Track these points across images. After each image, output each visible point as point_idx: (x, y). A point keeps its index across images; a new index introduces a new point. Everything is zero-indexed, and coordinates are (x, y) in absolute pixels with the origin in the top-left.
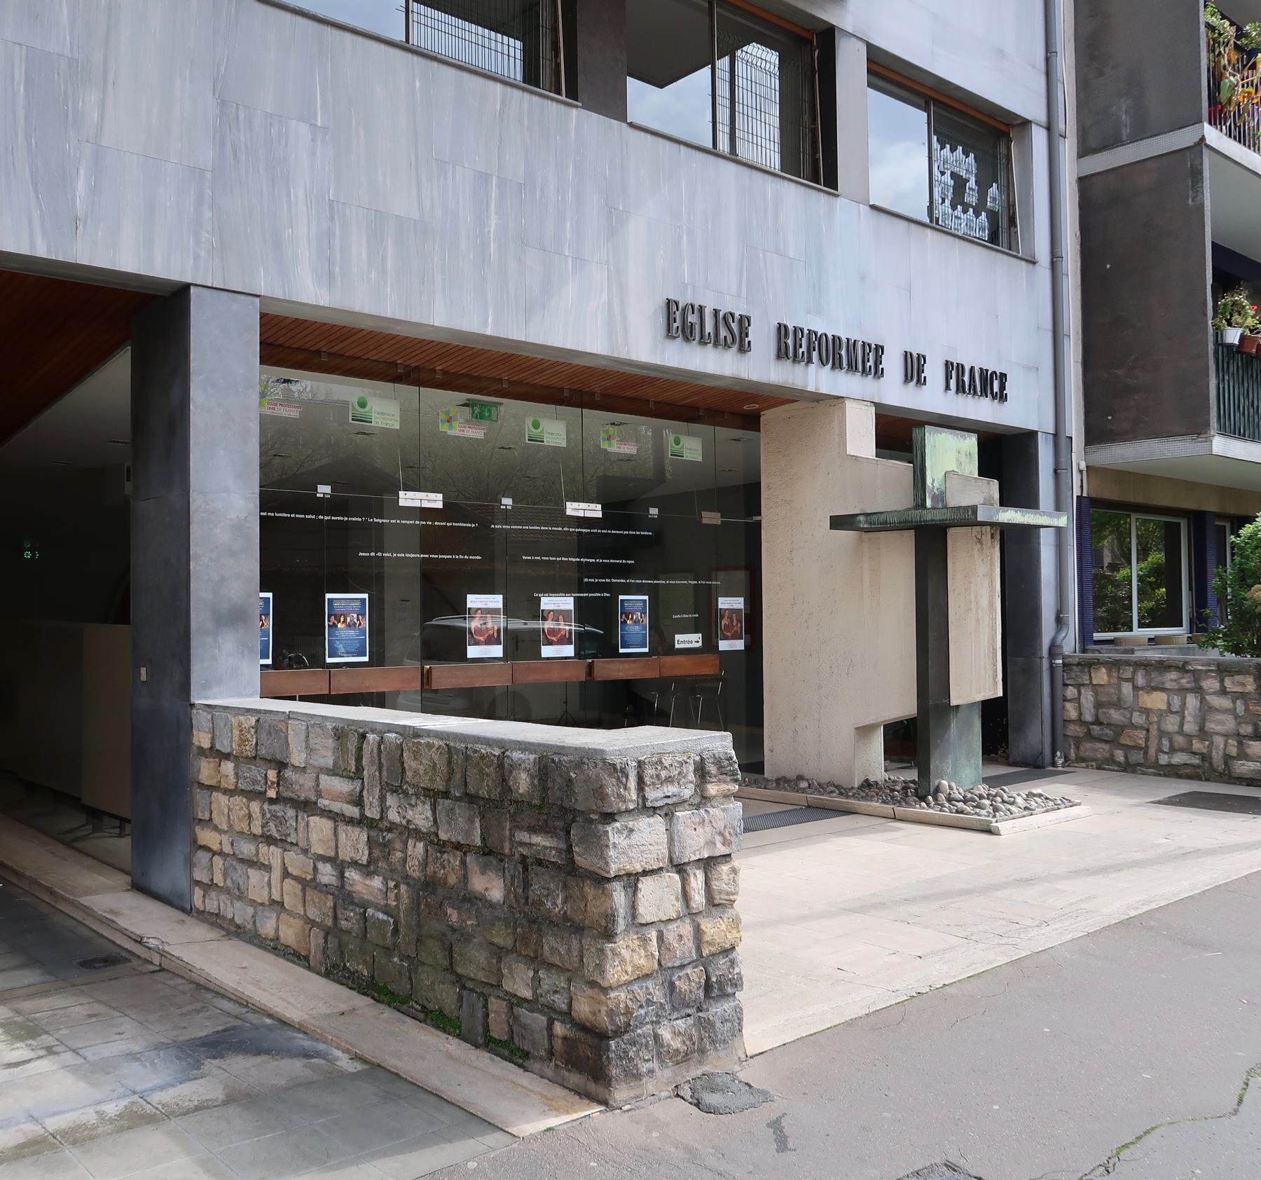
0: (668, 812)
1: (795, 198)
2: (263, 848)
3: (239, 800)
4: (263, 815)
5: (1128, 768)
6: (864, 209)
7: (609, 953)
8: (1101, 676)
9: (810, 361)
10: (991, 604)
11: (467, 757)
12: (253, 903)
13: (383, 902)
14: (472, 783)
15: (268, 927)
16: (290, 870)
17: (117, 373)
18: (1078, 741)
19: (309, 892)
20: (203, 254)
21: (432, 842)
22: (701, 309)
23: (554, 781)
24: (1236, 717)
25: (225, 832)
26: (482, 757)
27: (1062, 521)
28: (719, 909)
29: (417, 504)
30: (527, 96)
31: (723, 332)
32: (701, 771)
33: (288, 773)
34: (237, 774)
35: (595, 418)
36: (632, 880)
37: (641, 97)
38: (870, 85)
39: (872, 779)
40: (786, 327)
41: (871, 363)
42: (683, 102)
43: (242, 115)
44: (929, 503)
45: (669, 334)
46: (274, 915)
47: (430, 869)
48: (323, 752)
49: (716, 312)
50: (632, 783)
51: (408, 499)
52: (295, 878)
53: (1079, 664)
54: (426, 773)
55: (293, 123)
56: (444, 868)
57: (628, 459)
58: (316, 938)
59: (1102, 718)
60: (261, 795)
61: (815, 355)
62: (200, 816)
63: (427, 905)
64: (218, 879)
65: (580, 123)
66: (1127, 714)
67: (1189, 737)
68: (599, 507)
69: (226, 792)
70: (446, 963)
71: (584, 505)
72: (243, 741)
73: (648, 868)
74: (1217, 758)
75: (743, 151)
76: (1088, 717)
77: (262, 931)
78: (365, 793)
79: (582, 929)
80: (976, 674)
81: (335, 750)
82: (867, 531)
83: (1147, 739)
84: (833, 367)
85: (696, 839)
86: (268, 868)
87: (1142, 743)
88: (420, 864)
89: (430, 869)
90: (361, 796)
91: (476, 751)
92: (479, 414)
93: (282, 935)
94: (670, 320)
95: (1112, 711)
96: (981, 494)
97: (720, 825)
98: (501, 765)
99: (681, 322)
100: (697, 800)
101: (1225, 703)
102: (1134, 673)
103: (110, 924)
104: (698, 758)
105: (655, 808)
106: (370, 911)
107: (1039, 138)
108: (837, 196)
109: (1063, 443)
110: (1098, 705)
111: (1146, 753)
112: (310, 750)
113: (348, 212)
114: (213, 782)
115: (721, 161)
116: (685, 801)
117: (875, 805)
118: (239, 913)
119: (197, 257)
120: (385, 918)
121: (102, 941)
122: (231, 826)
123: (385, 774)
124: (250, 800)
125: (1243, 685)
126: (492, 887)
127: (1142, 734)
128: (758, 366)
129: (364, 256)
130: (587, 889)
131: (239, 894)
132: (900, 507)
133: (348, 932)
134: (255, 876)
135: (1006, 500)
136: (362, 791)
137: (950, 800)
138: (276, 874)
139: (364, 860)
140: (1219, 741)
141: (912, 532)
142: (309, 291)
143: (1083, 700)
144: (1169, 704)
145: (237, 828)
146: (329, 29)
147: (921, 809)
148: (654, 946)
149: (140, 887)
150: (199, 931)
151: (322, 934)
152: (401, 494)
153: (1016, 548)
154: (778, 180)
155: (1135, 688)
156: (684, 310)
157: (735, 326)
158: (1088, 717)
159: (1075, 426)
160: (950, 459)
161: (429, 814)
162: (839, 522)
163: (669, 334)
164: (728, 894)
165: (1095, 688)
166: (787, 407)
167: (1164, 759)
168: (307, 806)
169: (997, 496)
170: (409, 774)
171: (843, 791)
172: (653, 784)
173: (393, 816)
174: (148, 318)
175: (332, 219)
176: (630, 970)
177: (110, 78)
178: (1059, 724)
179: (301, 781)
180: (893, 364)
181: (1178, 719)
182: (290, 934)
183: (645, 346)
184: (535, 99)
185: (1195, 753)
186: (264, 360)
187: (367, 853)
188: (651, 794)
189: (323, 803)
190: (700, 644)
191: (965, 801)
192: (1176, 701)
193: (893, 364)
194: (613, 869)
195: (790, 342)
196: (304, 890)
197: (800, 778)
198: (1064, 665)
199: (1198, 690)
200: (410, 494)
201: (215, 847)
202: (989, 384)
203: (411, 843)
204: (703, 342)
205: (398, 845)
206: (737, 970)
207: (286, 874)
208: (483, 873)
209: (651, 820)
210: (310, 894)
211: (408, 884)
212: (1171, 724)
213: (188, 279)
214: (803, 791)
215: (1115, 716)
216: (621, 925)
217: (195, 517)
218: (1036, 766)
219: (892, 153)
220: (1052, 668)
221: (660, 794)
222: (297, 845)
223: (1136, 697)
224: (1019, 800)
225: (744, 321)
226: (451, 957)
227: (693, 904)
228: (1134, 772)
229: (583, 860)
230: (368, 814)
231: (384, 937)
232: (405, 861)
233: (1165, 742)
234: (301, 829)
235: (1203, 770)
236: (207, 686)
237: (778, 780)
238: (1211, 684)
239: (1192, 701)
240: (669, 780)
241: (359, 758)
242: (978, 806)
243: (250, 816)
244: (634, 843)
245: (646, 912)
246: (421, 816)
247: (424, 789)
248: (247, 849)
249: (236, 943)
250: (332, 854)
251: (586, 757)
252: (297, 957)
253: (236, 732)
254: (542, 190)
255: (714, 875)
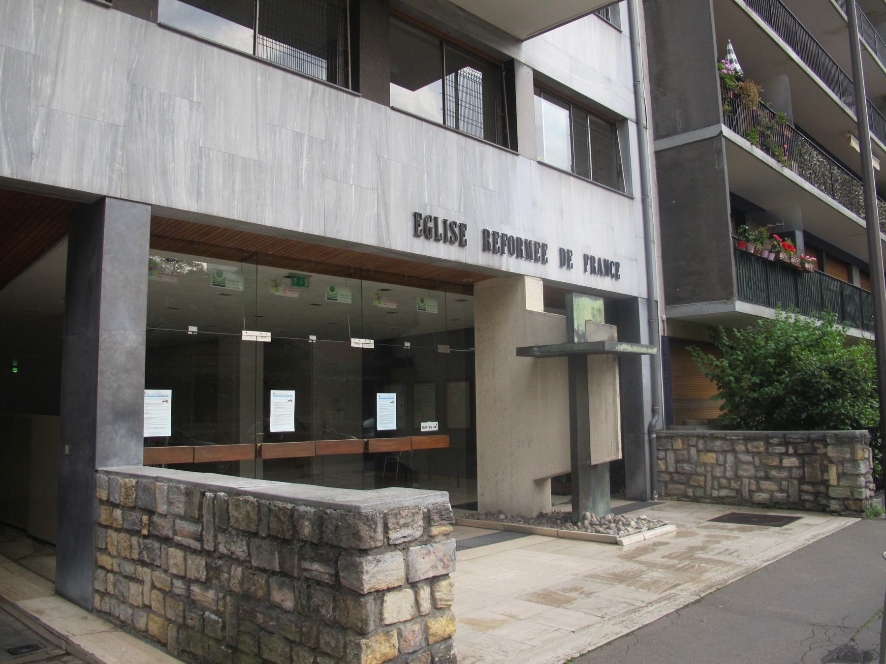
0: (404, 547)
1: (491, 154)
2: (139, 568)
3: (123, 535)
4: (140, 546)
5: (696, 500)
6: (534, 163)
7: (364, 647)
8: (679, 444)
9: (503, 253)
10: (615, 402)
11: (270, 510)
12: (132, 606)
13: (215, 608)
14: (277, 528)
15: (141, 622)
16: (156, 584)
17: (58, 257)
18: (666, 484)
19: (168, 599)
20: (115, 177)
21: (247, 567)
22: (436, 219)
23: (327, 527)
24: (755, 466)
25: (116, 557)
26: (280, 509)
27: (654, 351)
28: (441, 611)
29: (254, 339)
30: (328, 89)
31: (449, 234)
32: (428, 519)
33: (155, 518)
34: (123, 518)
35: (371, 286)
36: (380, 594)
37: (397, 92)
38: (535, 93)
39: (544, 512)
40: (488, 231)
41: (540, 254)
42: (427, 99)
43: (145, 94)
44: (576, 340)
45: (416, 235)
46: (146, 615)
47: (246, 586)
48: (177, 504)
49: (445, 222)
50: (380, 529)
51: (248, 336)
52: (159, 590)
53: (666, 437)
54: (243, 520)
55: (178, 99)
56: (255, 585)
57: (391, 312)
58: (172, 632)
59: (680, 470)
60: (137, 533)
61: (506, 248)
62: (100, 546)
63: (244, 610)
64: (110, 589)
65: (362, 107)
66: (694, 467)
67: (729, 480)
68: (372, 341)
69: (117, 530)
70: (256, 650)
71: (362, 341)
72: (128, 496)
73: (391, 586)
74: (746, 494)
75: (463, 127)
76: (671, 469)
77: (137, 626)
78: (204, 533)
79: (346, 629)
80: (606, 446)
81: (186, 502)
82: (539, 357)
83: (705, 481)
84: (517, 257)
85: (425, 563)
86: (141, 582)
87: (702, 484)
88: (239, 583)
89: (246, 586)
90: (201, 535)
91: (276, 506)
92: (299, 282)
93: (150, 629)
94: (416, 225)
95: (685, 465)
96: (606, 334)
97: (441, 554)
98: (292, 516)
99: (423, 226)
100: (425, 538)
101: (749, 458)
102: (697, 442)
103: (36, 620)
104: (425, 510)
105: (396, 545)
106: (207, 613)
107: (632, 128)
108: (517, 155)
109: (654, 304)
110: (677, 462)
111: (705, 491)
112: (170, 503)
113: (211, 155)
114: (108, 523)
115: (448, 132)
116: (416, 540)
117: (547, 529)
118: (123, 612)
119: (111, 179)
120: (216, 618)
121: (29, 632)
122: (119, 553)
123: (217, 520)
124: (132, 535)
125: (758, 447)
126: (285, 598)
127: (702, 478)
128: (472, 255)
129: (221, 181)
130: (349, 602)
131: (123, 600)
132: (559, 342)
133: (193, 628)
134: (134, 588)
135: (622, 338)
136: (202, 531)
137: (592, 524)
138: (147, 587)
139: (204, 578)
140: (746, 481)
141: (566, 358)
142: (183, 200)
143: (668, 459)
144: (717, 460)
145: (123, 554)
146: (204, 45)
147: (574, 531)
148: (395, 640)
149: (60, 593)
150: (98, 625)
151: (175, 629)
152: (244, 332)
153: (628, 366)
154: (482, 144)
155: (698, 451)
156: (425, 219)
157: (457, 230)
158: (671, 469)
159: (659, 294)
160: (587, 313)
161: (245, 548)
162: (522, 352)
163: (416, 235)
164: (446, 601)
165: (675, 451)
166: (488, 281)
167: (715, 493)
168: (167, 541)
169: (616, 335)
170: (232, 520)
171: (527, 520)
172: (395, 528)
173: (222, 549)
174: (77, 217)
175: (201, 158)
176: (378, 657)
177: (60, 68)
178: (655, 473)
179: (163, 524)
180: (553, 256)
181: (723, 469)
182: (154, 628)
183: (402, 240)
184: (333, 91)
185: (732, 489)
186: (152, 246)
187: (205, 573)
188: (393, 535)
189: (178, 538)
190: (437, 429)
191: (601, 525)
192: (721, 458)
193: (553, 256)
194: (366, 588)
195: (491, 240)
196: (164, 598)
197: (500, 512)
198: (658, 438)
199: (734, 451)
200: (250, 333)
201: (109, 567)
202: (609, 269)
203: (233, 568)
204: (437, 240)
205: (225, 569)
206: (452, 652)
207: (153, 587)
208: (280, 589)
209: (394, 553)
210: (169, 601)
211: (231, 595)
212: (718, 472)
213: (104, 193)
214: (502, 520)
215: (687, 467)
216: (372, 627)
217: (102, 346)
218: (642, 500)
219: (548, 127)
220: (650, 440)
221: (398, 535)
222: (160, 567)
223: (698, 456)
224: (633, 523)
225: (463, 227)
226: (259, 647)
227: (422, 609)
228: (698, 502)
229: (346, 580)
230: (206, 547)
231: (216, 632)
232: (229, 580)
233: (716, 483)
234: (163, 556)
235: (738, 500)
236: (107, 458)
237: (486, 514)
238: (740, 447)
239: (730, 458)
240: (406, 525)
241: (200, 508)
242: (608, 528)
243: (131, 547)
244: (380, 570)
245: (390, 616)
246: (240, 549)
247: (243, 531)
248: (129, 568)
249: (120, 634)
250: (183, 574)
251: (352, 511)
252: (161, 644)
253: (123, 490)
254: (336, 145)
255: (437, 588)
